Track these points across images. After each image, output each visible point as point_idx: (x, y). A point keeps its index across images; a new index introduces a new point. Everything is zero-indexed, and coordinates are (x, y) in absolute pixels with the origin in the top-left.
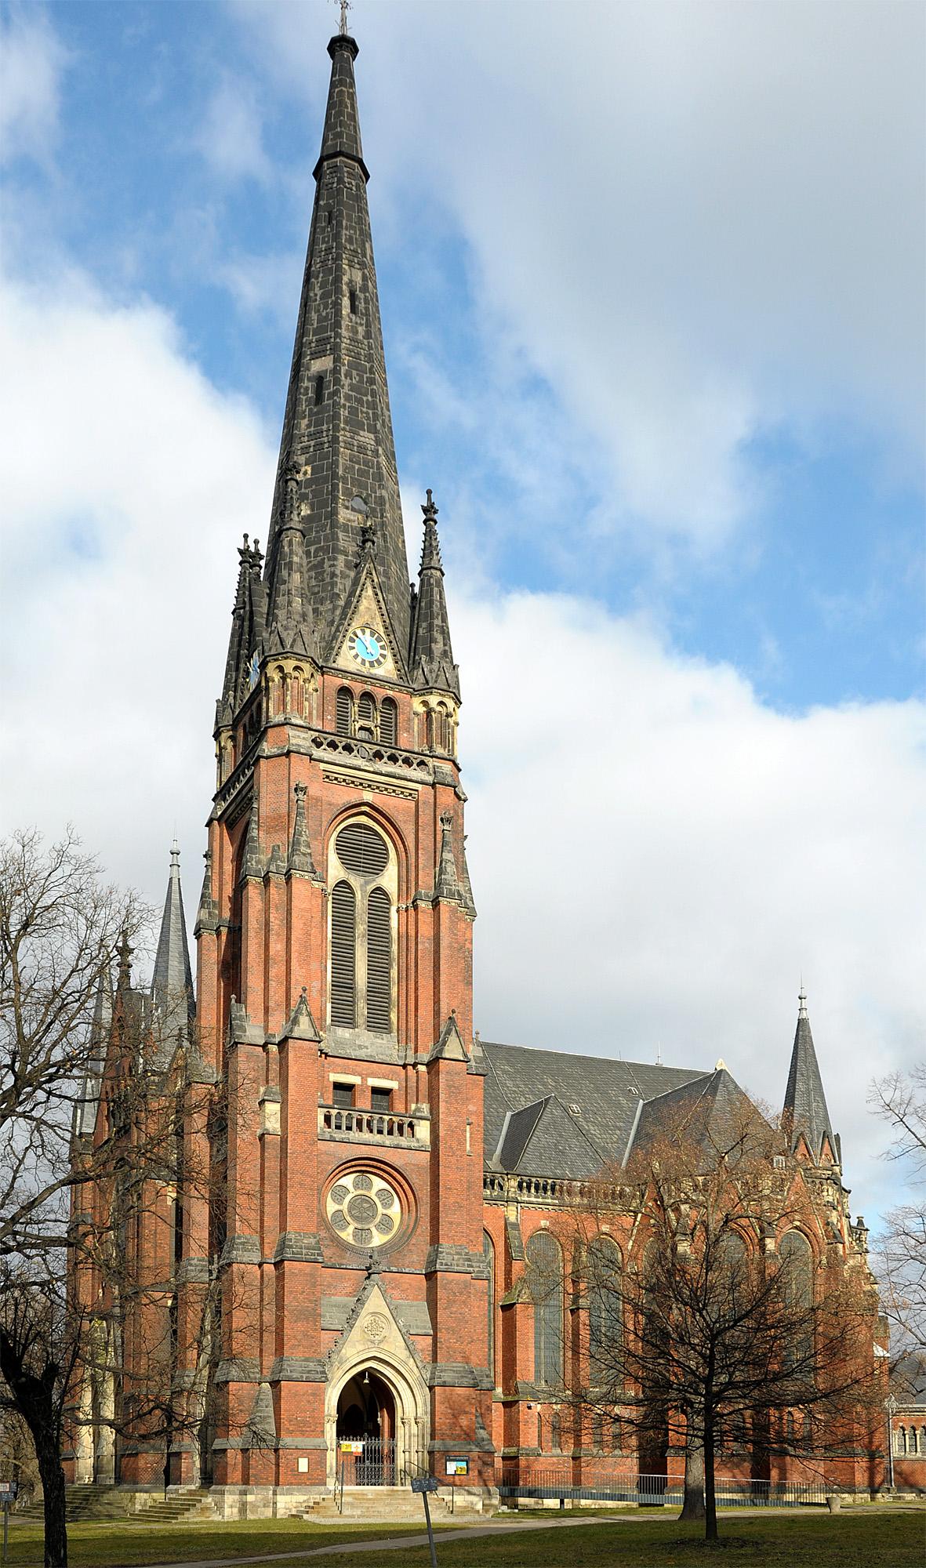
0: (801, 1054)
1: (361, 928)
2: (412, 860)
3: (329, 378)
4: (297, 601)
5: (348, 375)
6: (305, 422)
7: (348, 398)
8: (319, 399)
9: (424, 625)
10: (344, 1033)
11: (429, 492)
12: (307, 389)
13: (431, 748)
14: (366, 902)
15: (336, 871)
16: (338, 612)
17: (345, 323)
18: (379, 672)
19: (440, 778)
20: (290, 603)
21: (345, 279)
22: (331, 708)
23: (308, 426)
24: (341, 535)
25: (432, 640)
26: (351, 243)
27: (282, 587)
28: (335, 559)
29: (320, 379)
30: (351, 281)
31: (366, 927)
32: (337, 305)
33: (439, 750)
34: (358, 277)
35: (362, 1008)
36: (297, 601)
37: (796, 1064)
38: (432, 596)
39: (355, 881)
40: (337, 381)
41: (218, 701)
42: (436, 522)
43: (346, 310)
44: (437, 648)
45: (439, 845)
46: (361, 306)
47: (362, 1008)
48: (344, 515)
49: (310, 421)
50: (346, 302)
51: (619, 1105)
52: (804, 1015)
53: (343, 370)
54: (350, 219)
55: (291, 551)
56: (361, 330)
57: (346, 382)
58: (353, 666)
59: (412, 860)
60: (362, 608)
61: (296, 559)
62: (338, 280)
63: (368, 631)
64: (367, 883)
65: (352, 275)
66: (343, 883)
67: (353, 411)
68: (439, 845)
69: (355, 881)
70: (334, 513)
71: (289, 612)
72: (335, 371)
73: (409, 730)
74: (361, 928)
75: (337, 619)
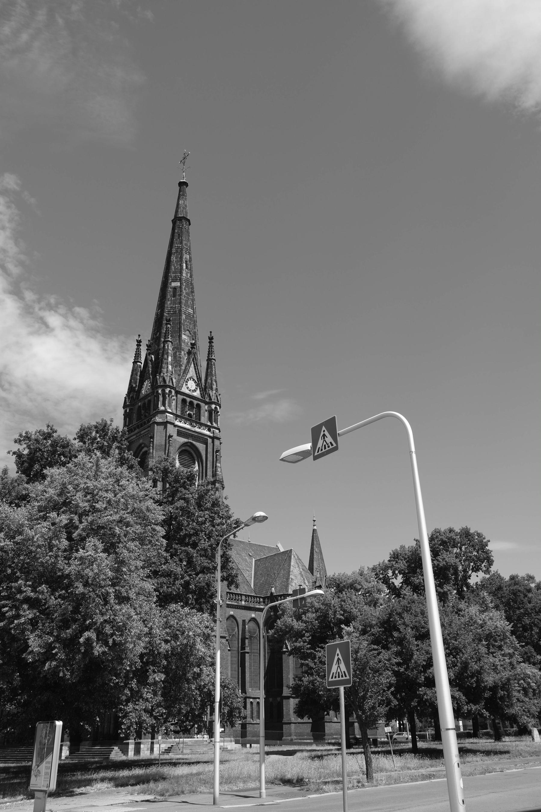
0: (315, 542)
2: (204, 465)
3: (178, 289)
4: (170, 367)
5: (185, 289)
6: (169, 302)
7: (185, 296)
8: (174, 296)
9: (209, 378)
11: (211, 332)
12: (170, 291)
13: (212, 423)
16: (182, 371)
17: (184, 272)
19: (215, 435)
20: (167, 367)
21: (184, 258)
22: (179, 406)
23: (171, 304)
24: (183, 344)
25: (212, 384)
26: (186, 246)
27: (165, 361)
28: (181, 352)
29: (175, 288)
30: (186, 258)
32: (181, 266)
33: (215, 425)
34: (188, 257)
36: (170, 367)
37: (313, 547)
38: (212, 368)
40: (181, 291)
41: (453, 528)
42: (213, 343)
43: (184, 267)
44: (214, 387)
45: (215, 460)
46: (189, 267)
48: (184, 337)
49: (171, 302)
50: (184, 265)
51: (246, 560)
52: (315, 528)
53: (184, 287)
54: (186, 238)
55: (168, 348)
56: (189, 275)
57: (184, 291)
58: (187, 391)
59: (204, 465)
60: (190, 371)
61: (170, 352)
62: (181, 258)
63: (192, 379)
65: (186, 256)
67: (187, 301)
68: (215, 460)
70: (180, 336)
71: (167, 370)
72: (181, 287)
73: (204, 416)
75: (182, 374)
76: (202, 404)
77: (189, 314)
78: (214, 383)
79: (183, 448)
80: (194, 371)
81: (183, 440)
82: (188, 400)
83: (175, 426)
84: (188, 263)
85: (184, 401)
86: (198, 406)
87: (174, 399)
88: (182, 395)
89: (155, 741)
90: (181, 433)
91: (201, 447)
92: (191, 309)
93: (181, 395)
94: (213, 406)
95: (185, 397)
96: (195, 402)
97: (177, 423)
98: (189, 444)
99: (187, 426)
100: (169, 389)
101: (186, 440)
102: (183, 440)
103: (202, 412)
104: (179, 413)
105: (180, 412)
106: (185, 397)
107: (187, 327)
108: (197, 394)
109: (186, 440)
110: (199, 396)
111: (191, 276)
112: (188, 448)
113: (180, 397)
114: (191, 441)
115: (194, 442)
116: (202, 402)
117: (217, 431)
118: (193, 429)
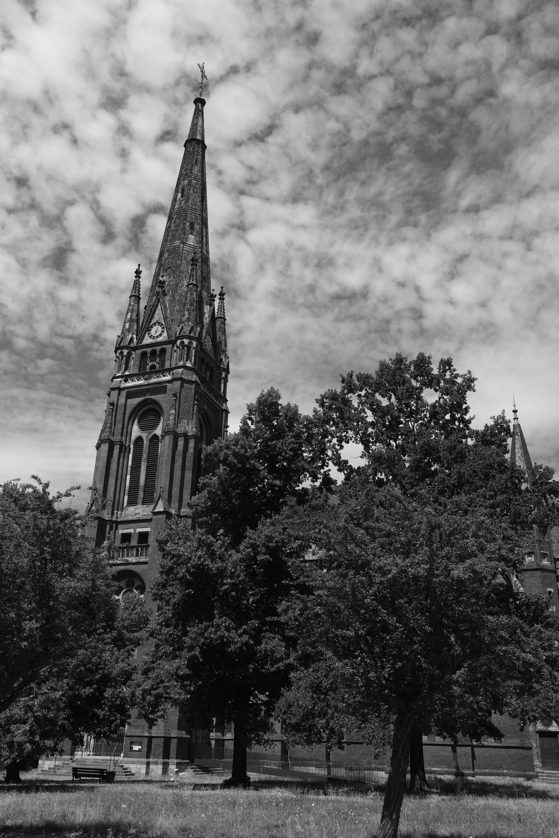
1: (145, 456)
10: (131, 509)
14: (148, 443)
15: (136, 431)
18: (160, 339)
31: (147, 455)
34: (186, 182)
35: (141, 494)
39: (144, 435)
46: (185, 193)
47: (141, 494)
56: (183, 202)
64: (149, 434)
66: (139, 439)
69: (144, 435)
74: (145, 456)
76: (168, 347)
77: (175, 247)
78: (186, 313)
79: (145, 409)
80: (161, 312)
81: (135, 401)
82: (149, 350)
83: (120, 389)
84: (186, 188)
85: (144, 354)
86: (163, 351)
87: (133, 358)
88: (141, 349)
89: (151, 760)
90: (131, 393)
91: (157, 397)
92: (179, 240)
93: (139, 349)
94: (179, 342)
95: (144, 350)
96: (158, 348)
97: (130, 384)
98: (149, 401)
99: (142, 382)
100: (120, 351)
101: (142, 399)
102: (135, 401)
103: (168, 355)
104: (136, 371)
105: (138, 370)
106: (144, 350)
107: (168, 265)
108: (164, 337)
109: (142, 399)
110: (167, 339)
111: (187, 202)
112: (151, 406)
113: (139, 352)
114: (149, 397)
115: (153, 397)
116: (167, 344)
117: (180, 370)
118: (146, 382)
